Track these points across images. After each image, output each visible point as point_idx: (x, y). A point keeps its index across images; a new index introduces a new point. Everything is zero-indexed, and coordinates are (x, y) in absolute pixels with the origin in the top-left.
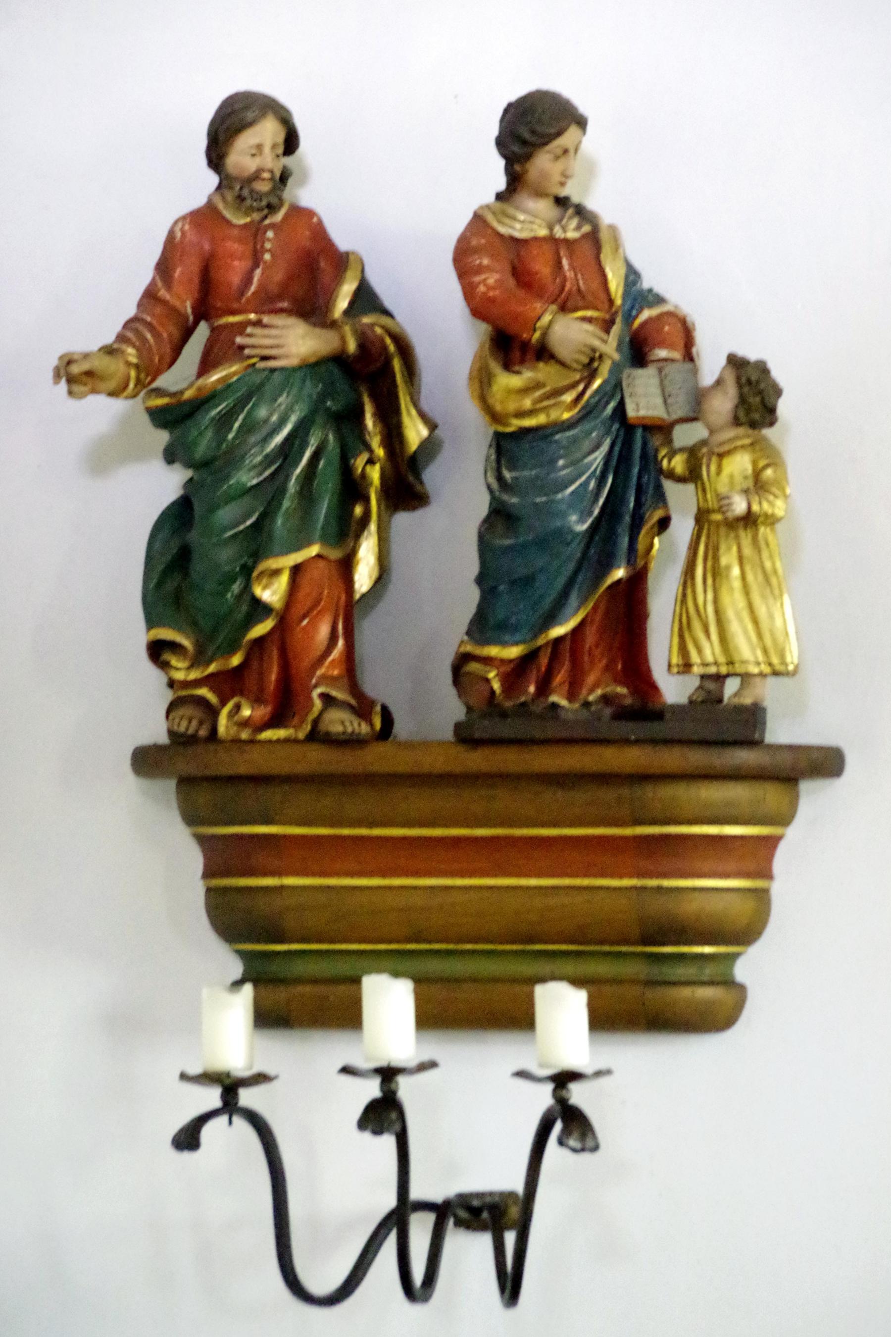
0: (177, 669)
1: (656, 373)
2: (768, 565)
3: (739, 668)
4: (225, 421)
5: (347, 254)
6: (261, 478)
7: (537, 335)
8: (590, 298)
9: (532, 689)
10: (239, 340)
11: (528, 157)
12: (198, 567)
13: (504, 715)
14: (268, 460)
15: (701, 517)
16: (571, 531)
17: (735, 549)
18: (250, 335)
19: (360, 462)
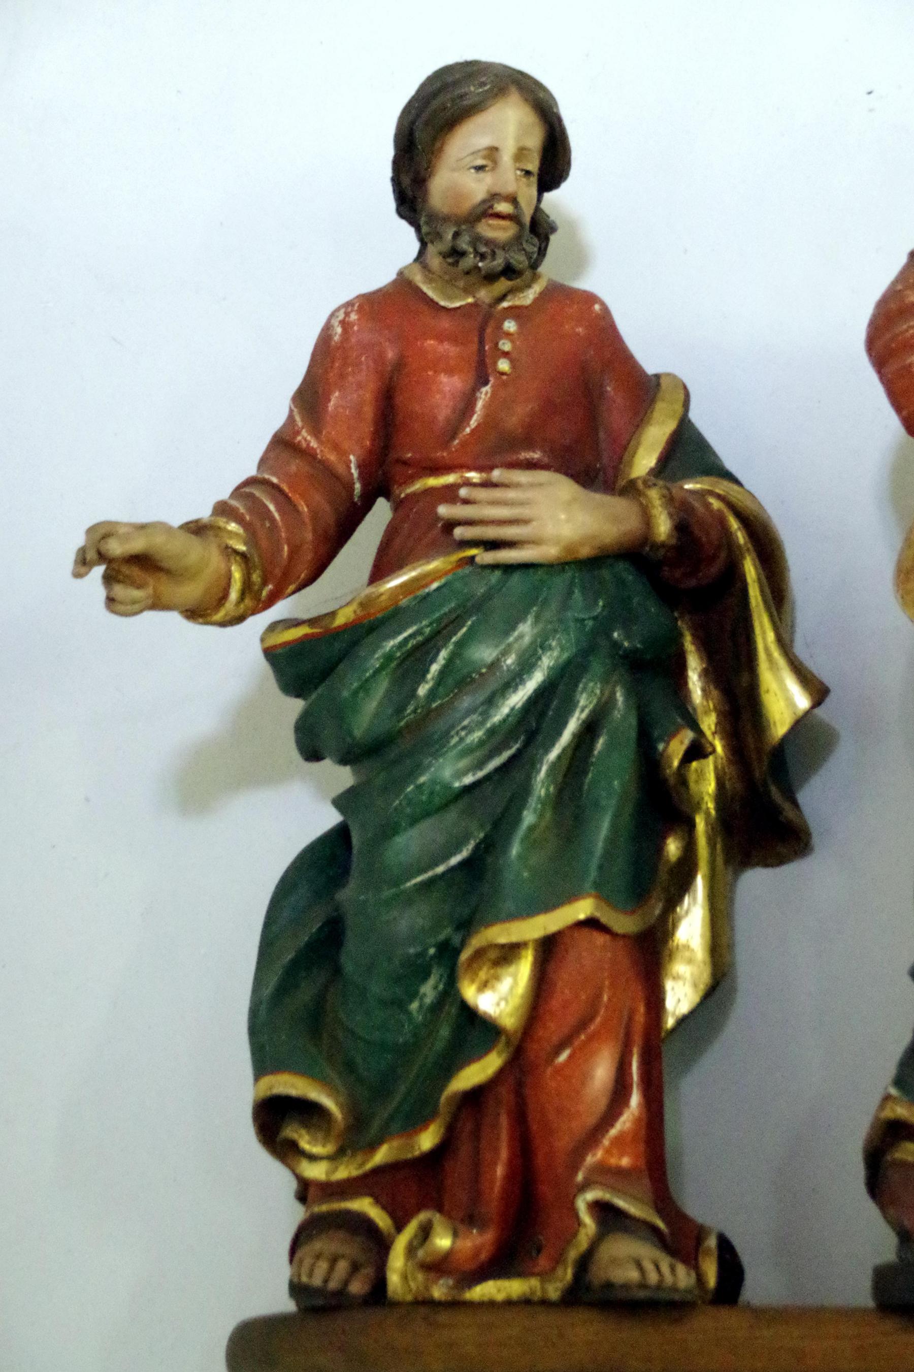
0: (312, 1158)
4: (415, 659)
5: (657, 376)
6: (480, 774)
10: (443, 510)
12: (351, 957)
14: (497, 738)
18: (466, 502)
19: (676, 749)
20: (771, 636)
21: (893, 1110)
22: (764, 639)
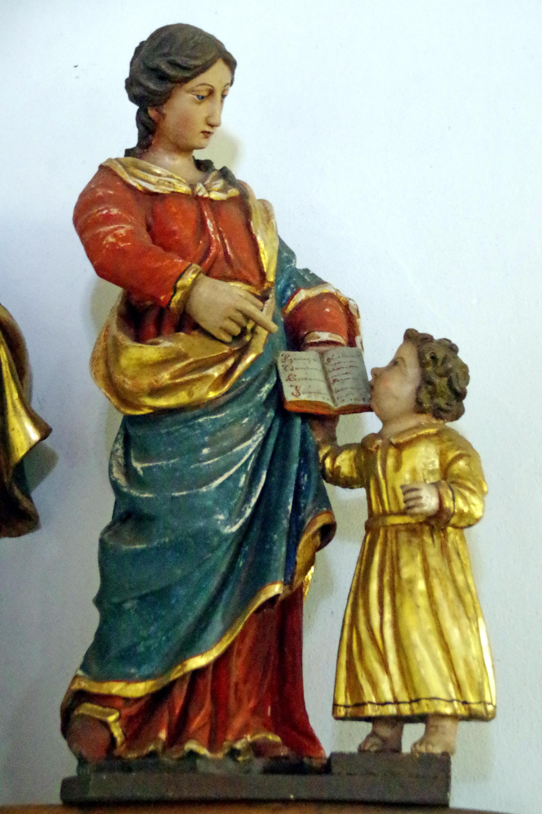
1: (317, 356)
2: (460, 578)
3: (425, 708)
7: (178, 296)
8: (237, 266)
9: (163, 735)
11: (165, 97)
13: (127, 767)
15: (373, 525)
16: (217, 532)
17: (419, 559)
20: (16, 395)
21: (79, 684)
22: (11, 397)
